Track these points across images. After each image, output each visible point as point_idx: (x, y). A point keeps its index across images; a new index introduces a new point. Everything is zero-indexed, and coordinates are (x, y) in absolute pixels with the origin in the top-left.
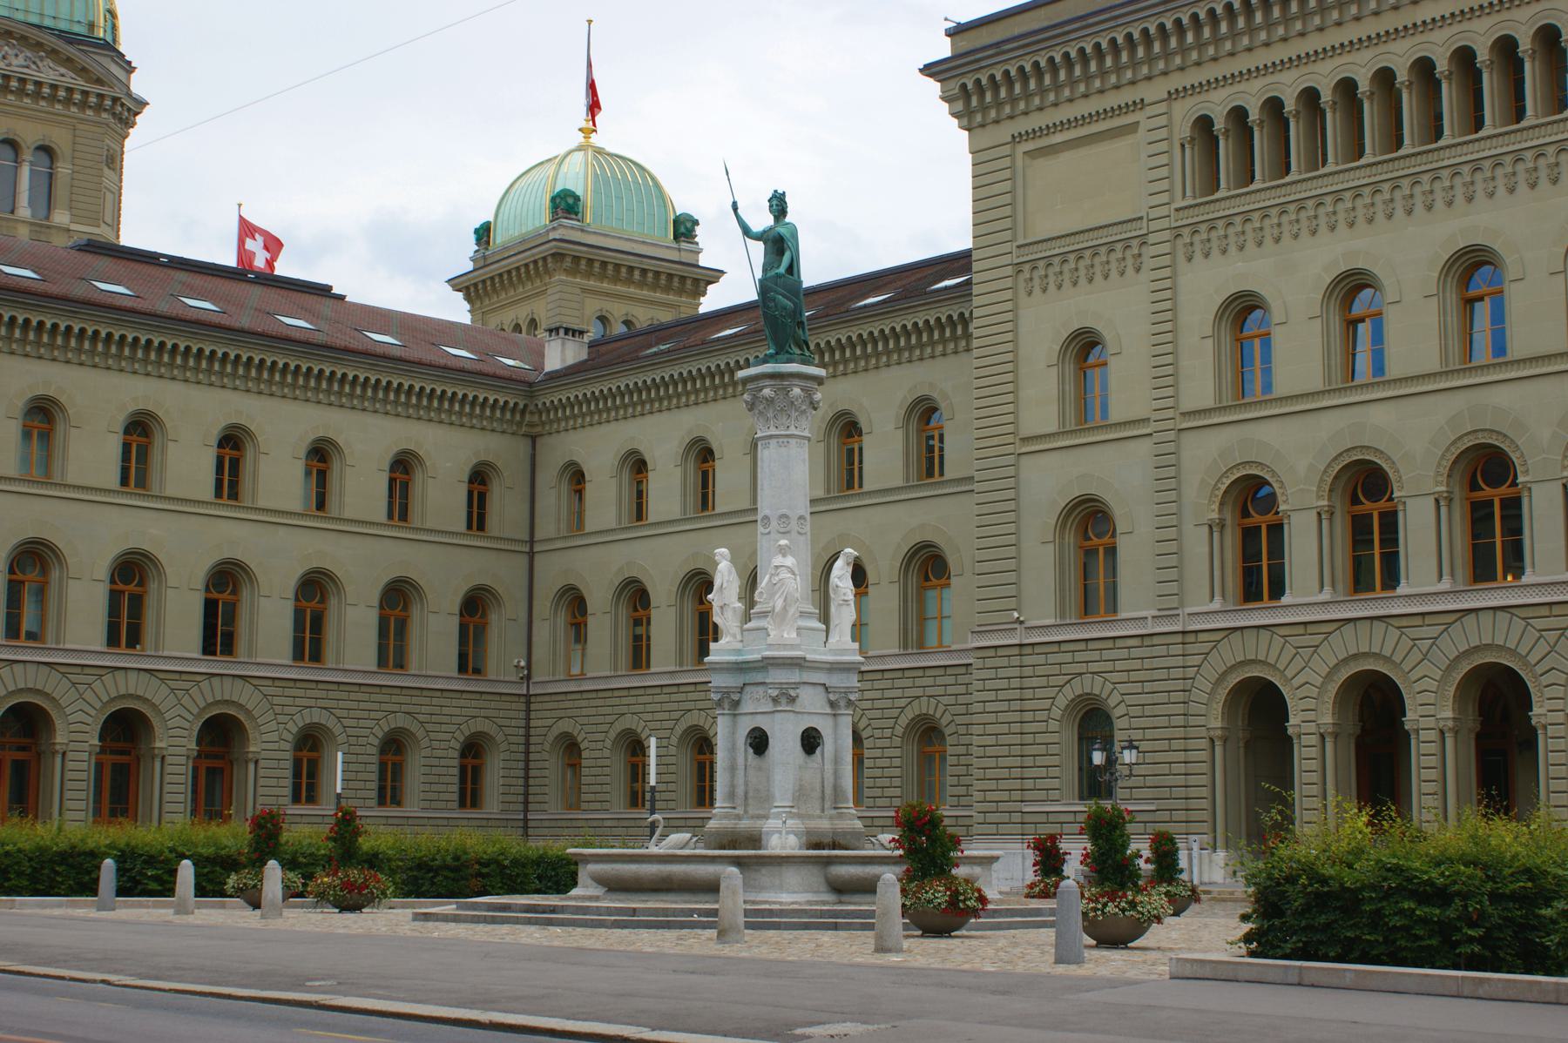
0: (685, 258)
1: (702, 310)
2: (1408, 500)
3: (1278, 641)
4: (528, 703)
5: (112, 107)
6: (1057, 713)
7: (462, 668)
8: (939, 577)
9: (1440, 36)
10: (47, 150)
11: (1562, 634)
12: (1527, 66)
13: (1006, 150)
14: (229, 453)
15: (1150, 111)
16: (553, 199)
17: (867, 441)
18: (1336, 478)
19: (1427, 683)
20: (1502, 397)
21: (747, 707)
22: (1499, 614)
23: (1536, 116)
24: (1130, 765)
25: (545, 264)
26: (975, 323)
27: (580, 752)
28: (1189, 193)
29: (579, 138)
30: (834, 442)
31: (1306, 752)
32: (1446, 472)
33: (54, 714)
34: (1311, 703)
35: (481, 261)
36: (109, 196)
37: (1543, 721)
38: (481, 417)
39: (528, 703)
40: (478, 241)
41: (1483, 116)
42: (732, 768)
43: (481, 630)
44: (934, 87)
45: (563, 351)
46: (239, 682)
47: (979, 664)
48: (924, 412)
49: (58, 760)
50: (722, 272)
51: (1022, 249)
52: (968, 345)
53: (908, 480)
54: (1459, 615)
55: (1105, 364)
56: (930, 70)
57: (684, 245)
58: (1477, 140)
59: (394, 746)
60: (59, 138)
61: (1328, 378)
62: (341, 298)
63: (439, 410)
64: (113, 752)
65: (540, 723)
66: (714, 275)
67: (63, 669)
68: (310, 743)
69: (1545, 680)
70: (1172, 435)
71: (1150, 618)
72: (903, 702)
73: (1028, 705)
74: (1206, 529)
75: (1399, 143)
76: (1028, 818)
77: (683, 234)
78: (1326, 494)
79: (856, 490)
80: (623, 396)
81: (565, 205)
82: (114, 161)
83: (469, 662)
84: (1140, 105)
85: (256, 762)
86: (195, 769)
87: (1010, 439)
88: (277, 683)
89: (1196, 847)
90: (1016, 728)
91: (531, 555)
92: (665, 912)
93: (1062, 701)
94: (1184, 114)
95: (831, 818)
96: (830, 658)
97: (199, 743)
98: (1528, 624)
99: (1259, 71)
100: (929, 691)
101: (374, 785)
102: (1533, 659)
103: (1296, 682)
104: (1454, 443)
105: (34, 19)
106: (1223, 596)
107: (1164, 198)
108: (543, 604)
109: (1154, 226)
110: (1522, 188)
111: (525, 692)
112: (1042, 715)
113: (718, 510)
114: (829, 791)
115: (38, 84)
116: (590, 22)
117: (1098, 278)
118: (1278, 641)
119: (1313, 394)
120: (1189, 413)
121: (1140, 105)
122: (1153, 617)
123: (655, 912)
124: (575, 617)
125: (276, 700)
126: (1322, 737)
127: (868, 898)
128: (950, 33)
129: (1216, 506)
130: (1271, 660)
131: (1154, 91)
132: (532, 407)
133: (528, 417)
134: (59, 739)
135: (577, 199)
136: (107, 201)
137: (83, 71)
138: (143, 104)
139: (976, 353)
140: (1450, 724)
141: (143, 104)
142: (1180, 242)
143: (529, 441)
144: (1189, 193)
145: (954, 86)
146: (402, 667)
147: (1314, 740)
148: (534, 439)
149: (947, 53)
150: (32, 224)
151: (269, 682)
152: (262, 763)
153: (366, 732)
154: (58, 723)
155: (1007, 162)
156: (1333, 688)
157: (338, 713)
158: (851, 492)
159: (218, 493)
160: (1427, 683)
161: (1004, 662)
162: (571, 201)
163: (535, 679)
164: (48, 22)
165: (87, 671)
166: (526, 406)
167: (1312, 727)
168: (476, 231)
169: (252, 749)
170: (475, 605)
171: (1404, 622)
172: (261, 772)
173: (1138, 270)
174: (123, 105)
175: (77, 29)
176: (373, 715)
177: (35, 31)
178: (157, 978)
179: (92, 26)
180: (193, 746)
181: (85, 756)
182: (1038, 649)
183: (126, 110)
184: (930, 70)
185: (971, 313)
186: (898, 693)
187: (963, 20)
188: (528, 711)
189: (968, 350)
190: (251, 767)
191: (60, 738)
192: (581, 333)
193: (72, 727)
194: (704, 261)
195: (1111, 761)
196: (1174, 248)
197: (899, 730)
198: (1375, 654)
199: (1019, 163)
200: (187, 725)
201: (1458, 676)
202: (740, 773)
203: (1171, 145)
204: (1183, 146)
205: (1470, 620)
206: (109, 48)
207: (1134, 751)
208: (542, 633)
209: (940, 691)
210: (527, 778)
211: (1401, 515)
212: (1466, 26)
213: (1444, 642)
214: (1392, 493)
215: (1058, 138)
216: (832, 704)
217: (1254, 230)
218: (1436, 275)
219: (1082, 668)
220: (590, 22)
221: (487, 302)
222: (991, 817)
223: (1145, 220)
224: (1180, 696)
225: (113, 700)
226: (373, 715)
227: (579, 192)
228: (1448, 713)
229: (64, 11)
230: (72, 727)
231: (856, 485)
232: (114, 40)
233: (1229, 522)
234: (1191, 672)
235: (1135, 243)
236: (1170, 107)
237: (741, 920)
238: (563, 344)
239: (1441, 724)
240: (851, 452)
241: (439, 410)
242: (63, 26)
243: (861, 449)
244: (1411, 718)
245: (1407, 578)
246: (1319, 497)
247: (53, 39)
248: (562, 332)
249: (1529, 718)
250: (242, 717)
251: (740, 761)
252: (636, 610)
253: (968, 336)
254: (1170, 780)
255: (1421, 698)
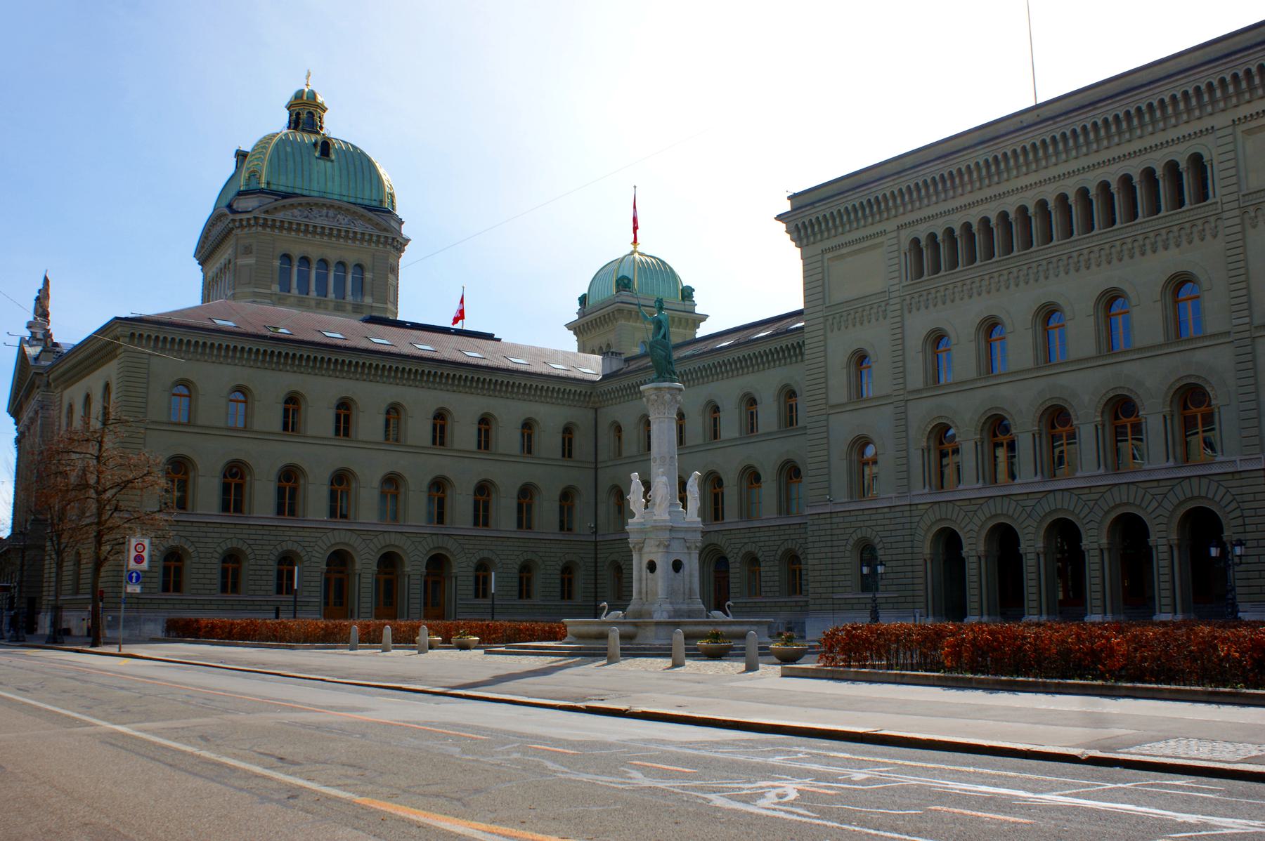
0: (688, 308)
1: (698, 336)
2: (1020, 435)
3: (957, 509)
4: (596, 546)
5: (392, 243)
6: (849, 547)
7: (562, 528)
8: (797, 477)
9: (993, 205)
10: (360, 267)
11: (1096, 503)
12: (1161, 183)
13: (1229, 130)
14: (439, 422)
15: (889, 236)
16: (617, 281)
17: (721, 414)
18: (930, 432)
19: (1030, 529)
20: (1199, 356)
21: (646, 549)
22: (1065, 493)
23: (1038, 246)
24: (1240, 556)
25: (614, 315)
26: (807, 347)
27: (622, 570)
28: (909, 278)
29: (632, 248)
30: (782, 399)
31: (1030, 563)
32: (1038, 420)
33: (354, 554)
34: (1163, 527)
35: (582, 313)
36: (392, 288)
37: (1087, 547)
38: (568, 399)
39: (596, 546)
40: (580, 304)
41: (1184, 199)
42: (640, 580)
43: (571, 508)
44: (782, 226)
45: (611, 364)
46: (447, 538)
47: (811, 522)
48: (789, 394)
49: (357, 578)
50: (707, 316)
51: (1247, 197)
52: (802, 358)
53: (780, 428)
54: (1045, 494)
55: (870, 367)
56: (780, 218)
57: (687, 303)
58: (1158, 219)
59: (526, 569)
60: (366, 260)
61: (926, 383)
62: (499, 340)
63: (546, 396)
64: (385, 574)
65: (602, 556)
66: (703, 318)
67: (358, 532)
68: (483, 568)
69: (1088, 526)
70: (1248, 341)
71: (1238, 462)
72: (779, 543)
73: (835, 543)
74: (920, 452)
75: (1113, 223)
76: (836, 602)
77: (686, 296)
78: (979, 432)
79: (795, 427)
80: (618, 391)
81: (624, 284)
82: (394, 270)
83: (565, 525)
84: (884, 232)
85: (456, 578)
86: (426, 582)
87: (823, 406)
88: (466, 537)
89: (918, 615)
90: (829, 555)
91: (596, 469)
92: (595, 649)
93: (851, 542)
94: (906, 236)
95: (688, 604)
96: (686, 526)
97: (427, 568)
98: (1220, 485)
99: (942, 214)
100: (792, 537)
101: (558, 590)
102: (1082, 516)
103: (966, 530)
104: (1041, 405)
105: (352, 200)
106: (930, 486)
107: (897, 281)
108: (603, 496)
109: (892, 296)
110: (1072, 272)
111: (594, 539)
112: (842, 549)
113: (687, 445)
114: (687, 590)
115: (355, 233)
116: (635, 187)
117: (866, 322)
118: (1013, 504)
119: (971, 380)
120: (914, 391)
121: (884, 232)
122: (1241, 460)
123: (590, 649)
124: (715, 488)
125: (467, 546)
126: (979, 557)
127: (604, 642)
128: (789, 198)
129: (925, 440)
130: (1210, 496)
131: (891, 225)
132: (594, 394)
133: (592, 399)
134: (357, 567)
135: (629, 280)
136: (388, 292)
137: (377, 225)
138: (408, 240)
139: (807, 362)
140: (929, 556)
141: (408, 240)
142: (1246, 216)
143: (594, 411)
144: (909, 278)
145: (792, 225)
146: (530, 528)
147: (975, 559)
148: (596, 410)
149: (789, 209)
150: (353, 304)
151: (462, 537)
152: (459, 578)
153: (268, 553)
154: (357, 559)
155: (1230, 139)
156: (984, 533)
157: (498, 552)
158: (792, 427)
159: (434, 443)
160: (1030, 529)
161: (823, 522)
162: (626, 281)
163: (600, 532)
164: (359, 201)
165: (370, 533)
166: (591, 393)
167: (1095, 546)
168: (579, 299)
169: (454, 571)
170: (567, 496)
171: (1019, 498)
172: (459, 583)
173: (885, 318)
174: (398, 241)
175: (374, 203)
176: (515, 553)
177: (352, 206)
178: (342, 678)
179: (381, 202)
180: (424, 570)
181: (370, 576)
182: (840, 515)
183: (399, 244)
184: (780, 218)
185: (804, 341)
186: (777, 538)
187: (797, 191)
188: (596, 549)
189: (802, 361)
190: (454, 580)
191: (358, 566)
192: (620, 354)
193: (364, 561)
194: (698, 310)
195: (1224, 553)
196: (1243, 220)
197: (778, 557)
198: (944, 519)
199: (826, 264)
200: (420, 559)
201: (1045, 525)
202: (644, 582)
203: (900, 253)
204: (905, 254)
205: (1051, 496)
206: (390, 213)
207: (883, 567)
208: (602, 509)
209: (797, 536)
210: (596, 584)
211: (1144, 425)
212: (1042, 188)
213: (979, 513)
214: (1210, 401)
215: (844, 251)
216: (688, 548)
217: (1250, 218)
218: (1031, 318)
219: (861, 524)
220: (635, 187)
221: (593, 332)
222: (817, 602)
223: (1220, 203)
224: (909, 538)
225: (383, 548)
226: (515, 553)
227: (631, 277)
228: (1041, 545)
229: (367, 195)
230: (364, 561)
231: (755, 430)
232: (393, 208)
233: (932, 448)
234: (914, 525)
235: (1212, 219)
236: (899, 233)
237: (619, 652)
238: (611, 361)
239: (1038, 550)
240: (791, 406)
241: (546, 396)
242: (366, 202)
243: (796, 404)
244: (1153, 539)
245: (1081, 468)
246: (975, 434)
247: (362, 210)
248: (610, 354)
249: (1081, 546)
250: (448, 555)
251: (644, 576)
252: (715, 488)
253: (802, 354)
254: (905, 581)
255: (1028, 537)
